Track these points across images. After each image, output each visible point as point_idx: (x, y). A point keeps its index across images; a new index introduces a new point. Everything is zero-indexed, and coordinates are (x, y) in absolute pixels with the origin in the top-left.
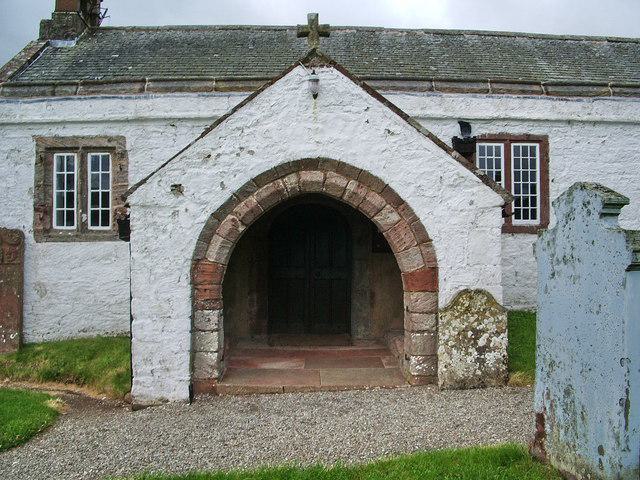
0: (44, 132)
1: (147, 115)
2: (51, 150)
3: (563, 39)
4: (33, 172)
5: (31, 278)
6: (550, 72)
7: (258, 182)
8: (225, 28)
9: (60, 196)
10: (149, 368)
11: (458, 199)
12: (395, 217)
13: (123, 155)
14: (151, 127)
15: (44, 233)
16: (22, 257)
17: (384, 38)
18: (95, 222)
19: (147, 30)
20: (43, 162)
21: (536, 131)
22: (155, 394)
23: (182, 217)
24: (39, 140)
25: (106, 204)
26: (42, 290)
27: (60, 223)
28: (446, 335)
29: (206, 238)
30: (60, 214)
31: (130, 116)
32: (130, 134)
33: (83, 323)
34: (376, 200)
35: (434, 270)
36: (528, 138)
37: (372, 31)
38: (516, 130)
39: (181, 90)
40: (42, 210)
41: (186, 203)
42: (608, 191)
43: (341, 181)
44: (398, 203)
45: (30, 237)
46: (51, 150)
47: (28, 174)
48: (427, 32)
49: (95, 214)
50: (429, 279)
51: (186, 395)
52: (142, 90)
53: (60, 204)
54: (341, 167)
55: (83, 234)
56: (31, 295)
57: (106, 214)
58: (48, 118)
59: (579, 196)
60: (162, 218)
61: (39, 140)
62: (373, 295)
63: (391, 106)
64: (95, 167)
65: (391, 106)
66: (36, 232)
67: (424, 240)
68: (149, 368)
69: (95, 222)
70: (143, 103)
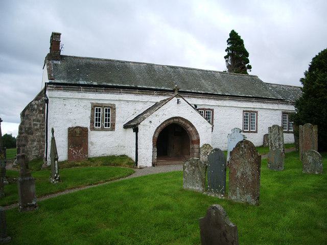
0: (94, 102)
1: (121, 99)
2: (95, 106)
3: (207, 71)
4: (90, 112)
5: (89, 140)
6: (209, 87)
7: (166, 121)
8: (106, 60)
9: (96, 119)
10: (144, 160)
11: (204, 126)
12: (192, 129)
13: (115, 109)
14: (122, 102)
15: (93, 129)
16: (87, 135)
17: (156, 68)
18: (106, 126)
19: (83, 58)
20: (93, 109)
21: (211, 108)
22: (144, 165)
23: (151, 128)
24: (92, 103)
25: (109, 121)
26: (92, 144)
27: (96, 126)
28: (202, 153)
29: (155, 132)
30: (96, 124)
31: (118, 99)
32: (117, 104)
33: (103, 153)
34: (188, 125)
35: (199, 140)
36: (209, 109)
37: (152, 65)
38: (207, 107)
39: (130, 93)
40: (92, 122)
41: (152, 125)
42: (173, 91)
43: (182, 121)
44: (192, 126)
45: (89, 130)
46: (95, 106)
47: (89, 113)
48: (168, 66)
49: (106, 124)
50: (198, 141)
51: (151, 165)
52: (120, 93)
53: (96, 121)
54: (182, 119)
55: (103, 129)
56: (89, 145)
57: (109, 124)
58: (95, 98)
59: (236, 130)
60: (147, 128)
61: (92, 103)
62: (174, 146)
63: (186, 101)
64: (106, 111)
65: (186, 101)
66: (91, 128)
67: (197, 134)
68: (144, 160)
69: (106, 126)
70: (121, 96)
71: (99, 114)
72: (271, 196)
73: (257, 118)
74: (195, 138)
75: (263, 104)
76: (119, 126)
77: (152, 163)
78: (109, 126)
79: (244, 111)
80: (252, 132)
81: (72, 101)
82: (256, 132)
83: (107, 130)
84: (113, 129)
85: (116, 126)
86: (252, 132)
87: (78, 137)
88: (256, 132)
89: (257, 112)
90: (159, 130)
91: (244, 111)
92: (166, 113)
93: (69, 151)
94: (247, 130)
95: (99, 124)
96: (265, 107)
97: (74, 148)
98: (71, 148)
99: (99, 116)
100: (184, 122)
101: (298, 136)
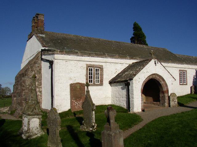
14: (107, 63)
20: (87, 69)
34: (161, 80)
35: (168, 91)
61: (87, 65)
67: (167, 86)
71: (92, 73)
72: (95, 138)
73: (186, 75)
74: (165, 89)
75: (189, 65)
76: (106, 82)
77: (142, 109)
78: (98, 82)
79: (180, 70)
80: (184, 84)
81: (72, 62)
82: (186, 84)
83: (97, 85)
84: (101, 84)
85: (104, 82)
86: (184, 84)
87: (78, 92)
88: (186, 84)
89: (186, 71)
90: (162, 83)
91: (180, 70)
92: (148, 71)
93: (72, 103)
94: (185, 83)
95: (92, 80)
96: (191, 68)
97: (76, 100)
98: (73, 100)
99: (92, 75)
100: (158, 78)
101: (8, 98)
